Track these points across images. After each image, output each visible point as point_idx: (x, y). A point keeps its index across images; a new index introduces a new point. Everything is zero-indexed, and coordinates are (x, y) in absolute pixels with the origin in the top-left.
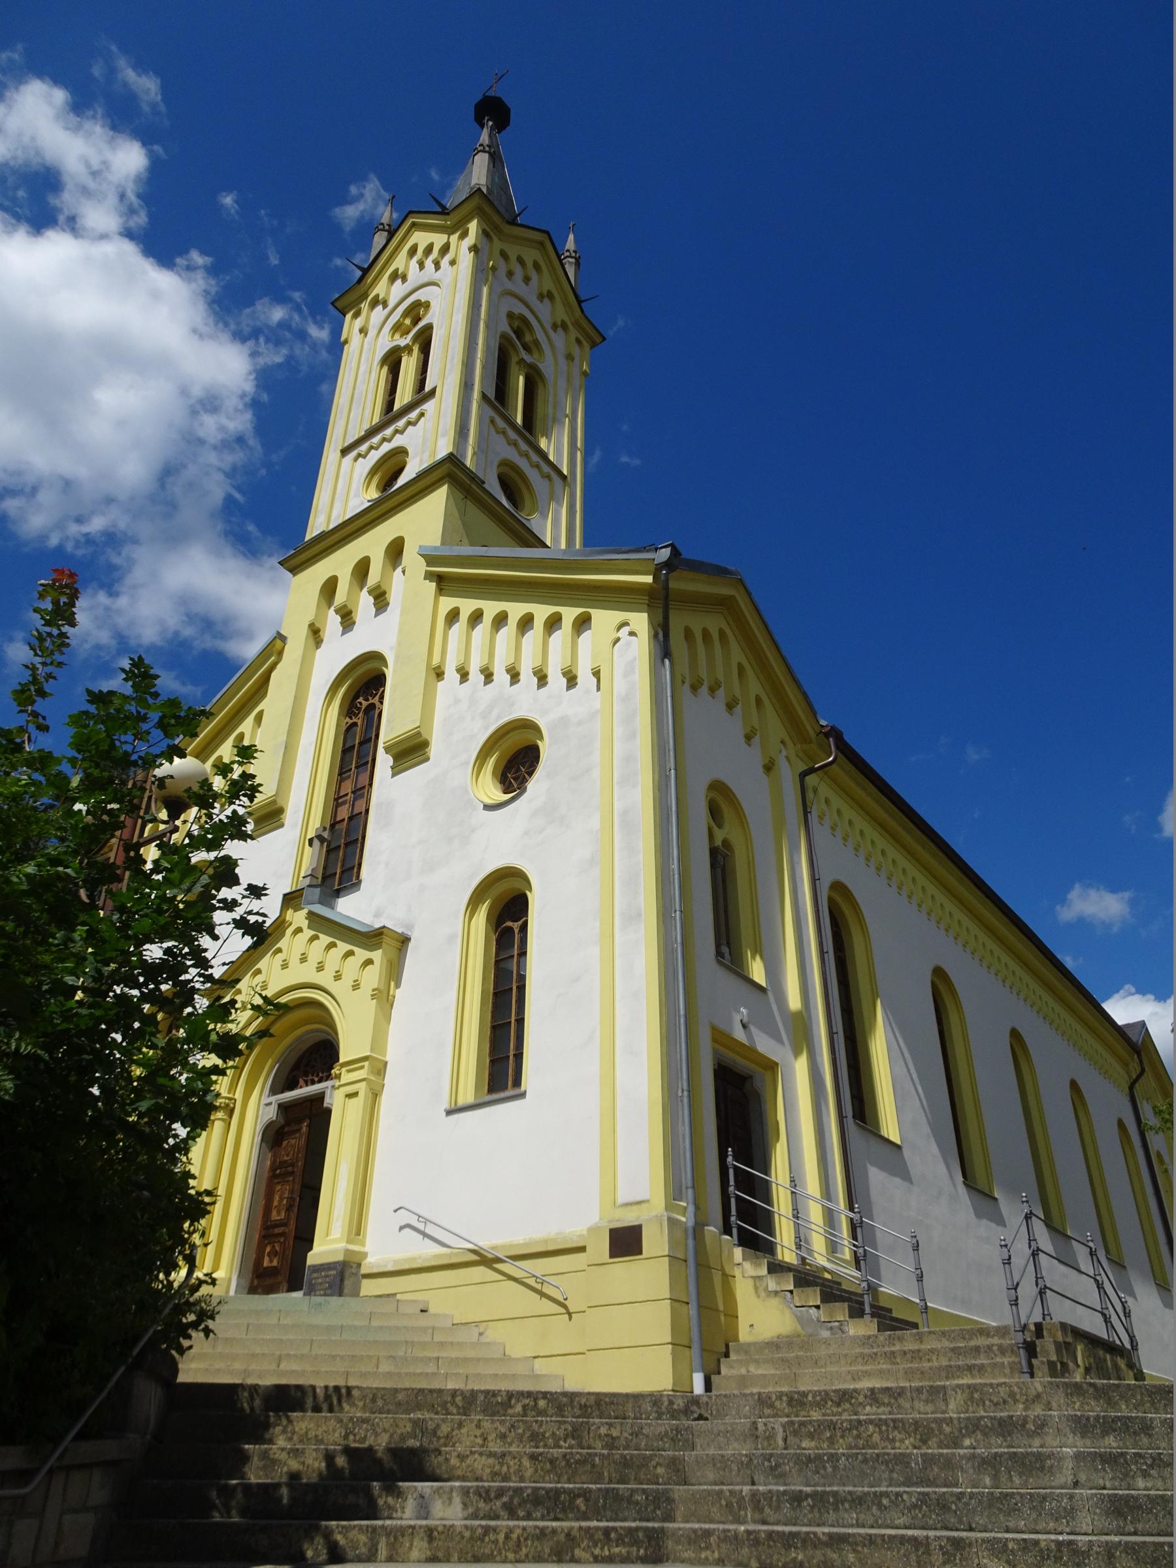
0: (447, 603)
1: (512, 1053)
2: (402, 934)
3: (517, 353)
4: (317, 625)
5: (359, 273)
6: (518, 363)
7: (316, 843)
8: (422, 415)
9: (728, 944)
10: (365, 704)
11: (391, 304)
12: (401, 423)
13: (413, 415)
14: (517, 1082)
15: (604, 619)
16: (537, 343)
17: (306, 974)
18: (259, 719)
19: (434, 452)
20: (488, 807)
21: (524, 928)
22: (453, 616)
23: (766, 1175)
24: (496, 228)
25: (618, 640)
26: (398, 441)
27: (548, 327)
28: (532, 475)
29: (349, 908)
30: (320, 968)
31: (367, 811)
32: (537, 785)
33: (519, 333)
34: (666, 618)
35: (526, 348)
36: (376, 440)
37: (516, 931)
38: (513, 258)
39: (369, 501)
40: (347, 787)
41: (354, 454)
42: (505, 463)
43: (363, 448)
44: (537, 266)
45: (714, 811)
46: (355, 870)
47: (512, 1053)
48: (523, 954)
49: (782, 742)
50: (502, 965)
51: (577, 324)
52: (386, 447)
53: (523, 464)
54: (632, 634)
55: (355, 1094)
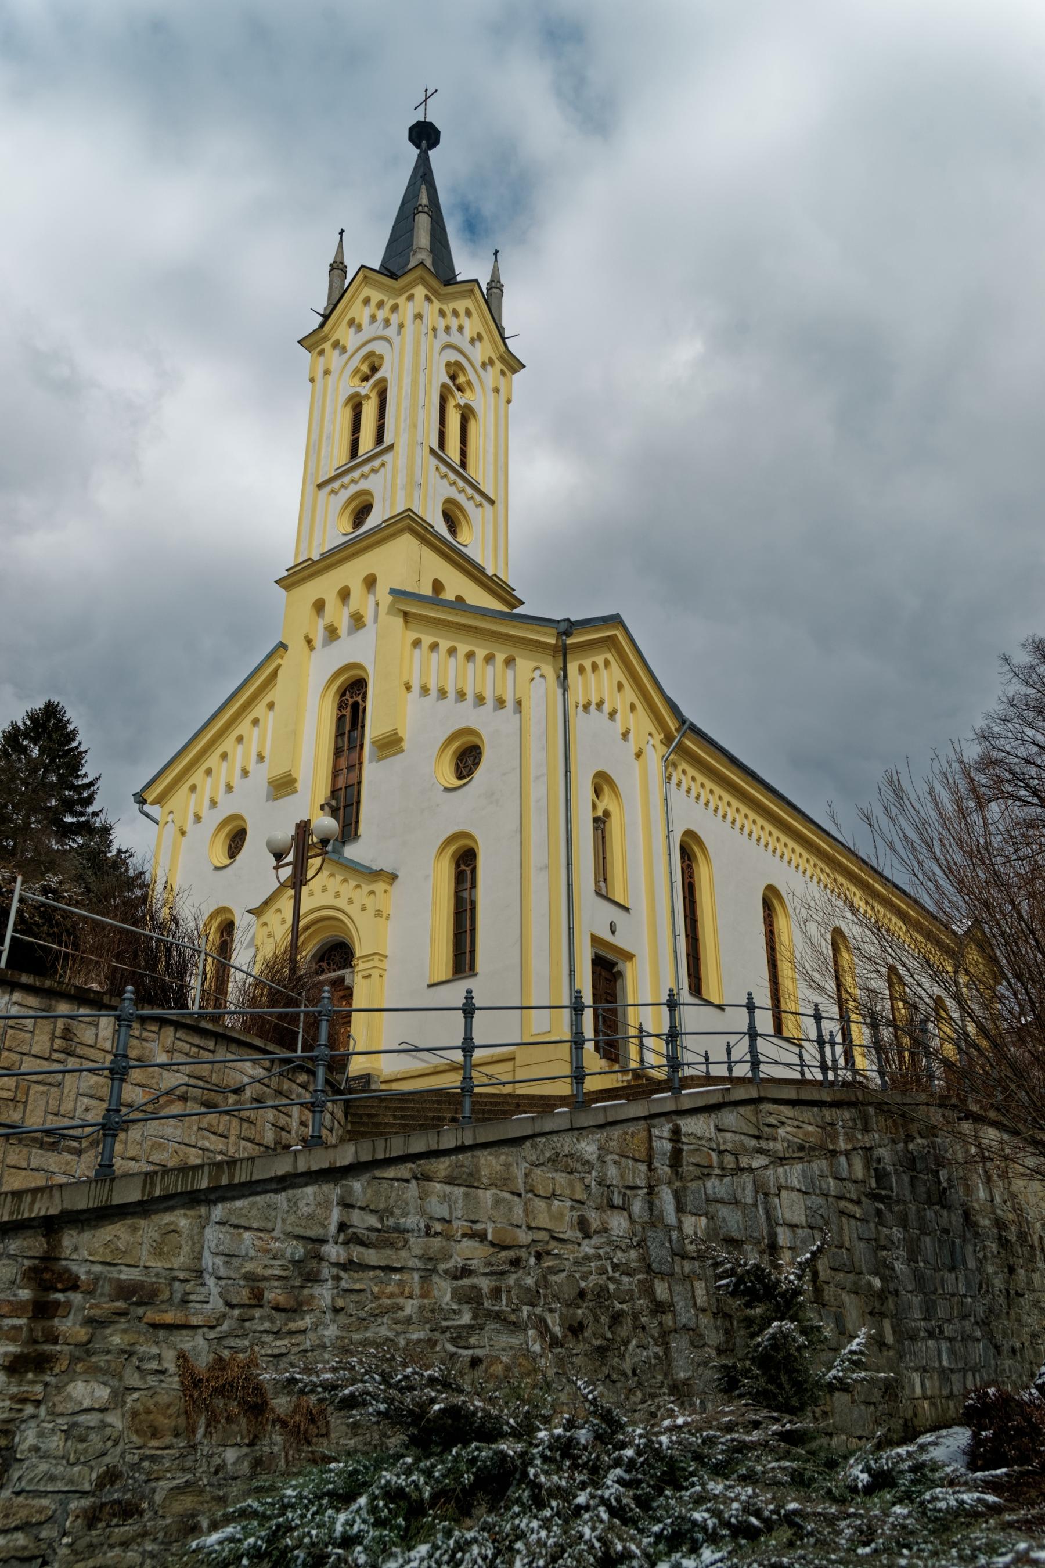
0: (413, 636)
1: (468, 950)
2: (392, 874)
3: (454, 397)
4: (311, 637)
5: (321, 319)
6: (455, 406)
7: (326, 808)
8: (383, 465)
9: (605, 880)
10: (351, 701)
11: (350, 349)
12: (366, 469)
13: (376, 463)
14: (472, 967)
15: (524, 665)
16: (469, 383)
17: (328, 899)
18: (271, 706)
19: (392, 505)
20: (447, 790)
21: (474, 871)
22: (417, 643)
23: (225, 958)
24: (435, 293)
25: (533, 679)
26: (363, 485)
27: (478, 365)
28: (468, 506)
29: (351, 852)
30: (337, 895)
31: (359, 783)
32: (479, 774)
33: (453, 378)
34: (565, 669)
35: (460, 389)
36: (346, 479)
37: (469, 872)
38: (449, 313)
39: (344, 535)
40: (343, 763)
41: (328, 489)
42: (449, 501)
43: (336, 485)
44: (468, 313)
45: (598, 792)
46: (353, 825)
47: (468, 950)
48: (474, 886)
49: (650, 734)
50: (460, 894)
51: (502, 359)
52: (353, 489)
53: (461, 499)
54: (542, 676)
55: (369, 976)
